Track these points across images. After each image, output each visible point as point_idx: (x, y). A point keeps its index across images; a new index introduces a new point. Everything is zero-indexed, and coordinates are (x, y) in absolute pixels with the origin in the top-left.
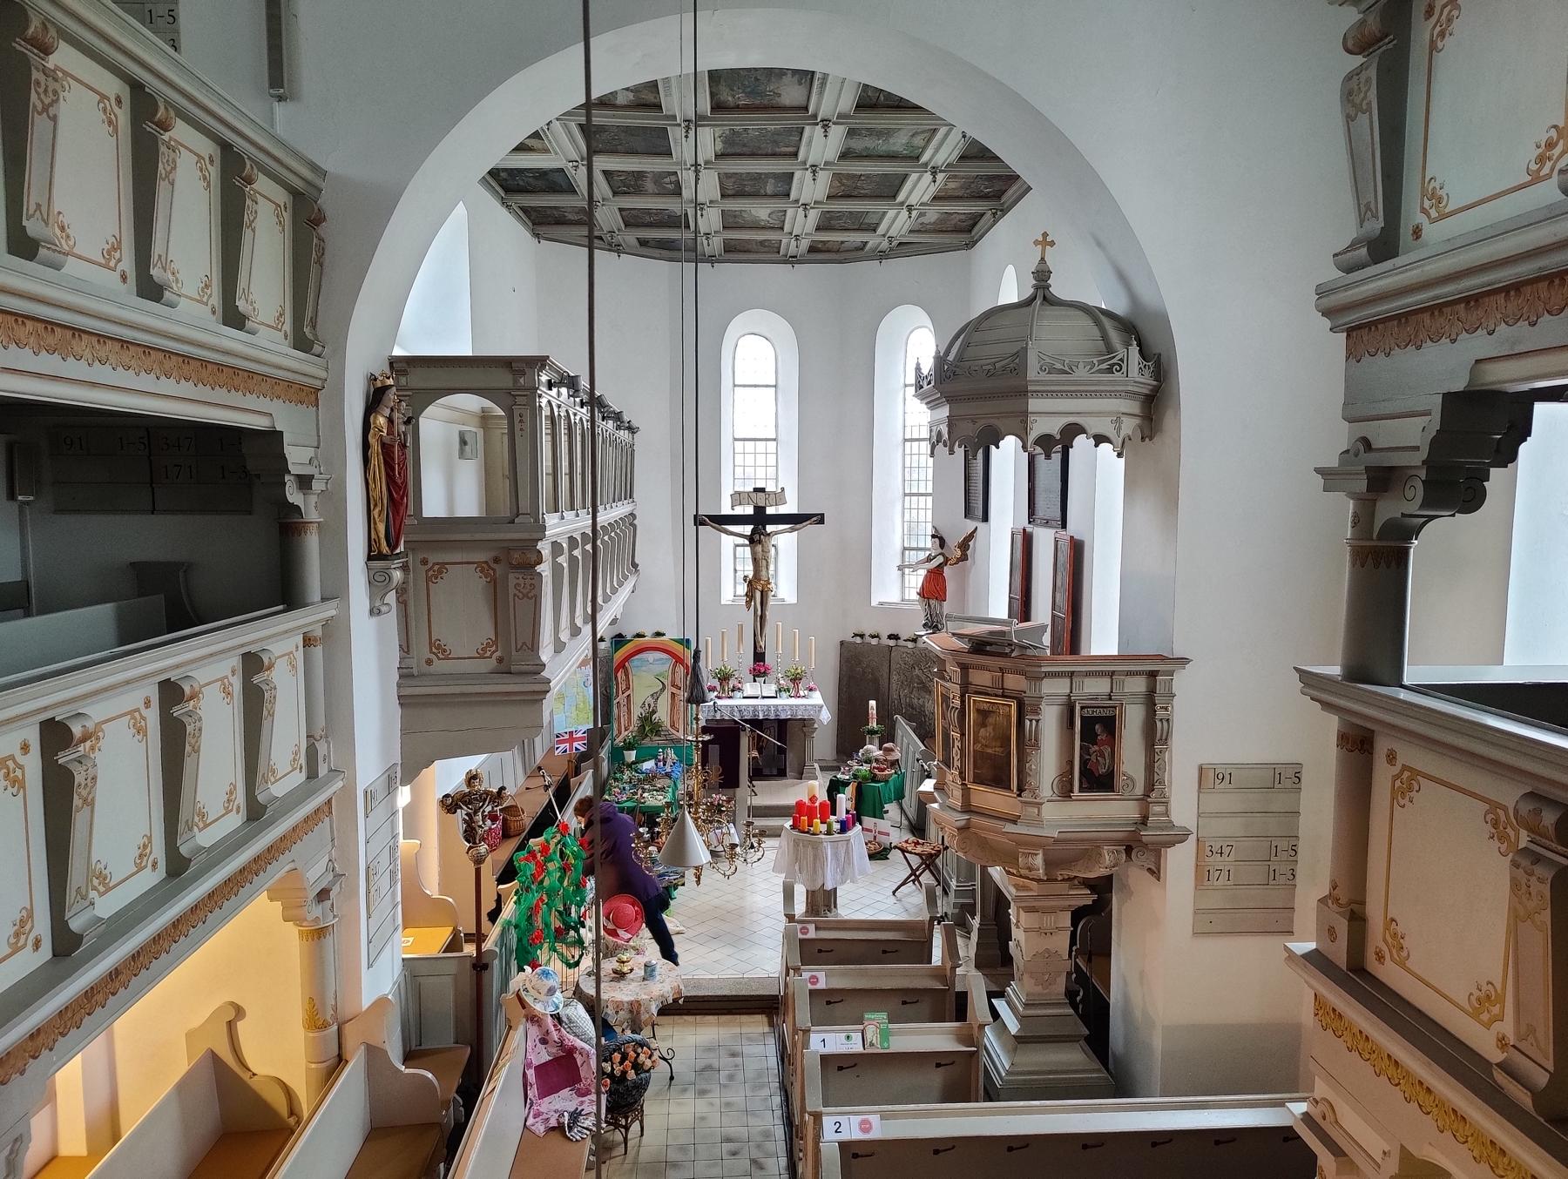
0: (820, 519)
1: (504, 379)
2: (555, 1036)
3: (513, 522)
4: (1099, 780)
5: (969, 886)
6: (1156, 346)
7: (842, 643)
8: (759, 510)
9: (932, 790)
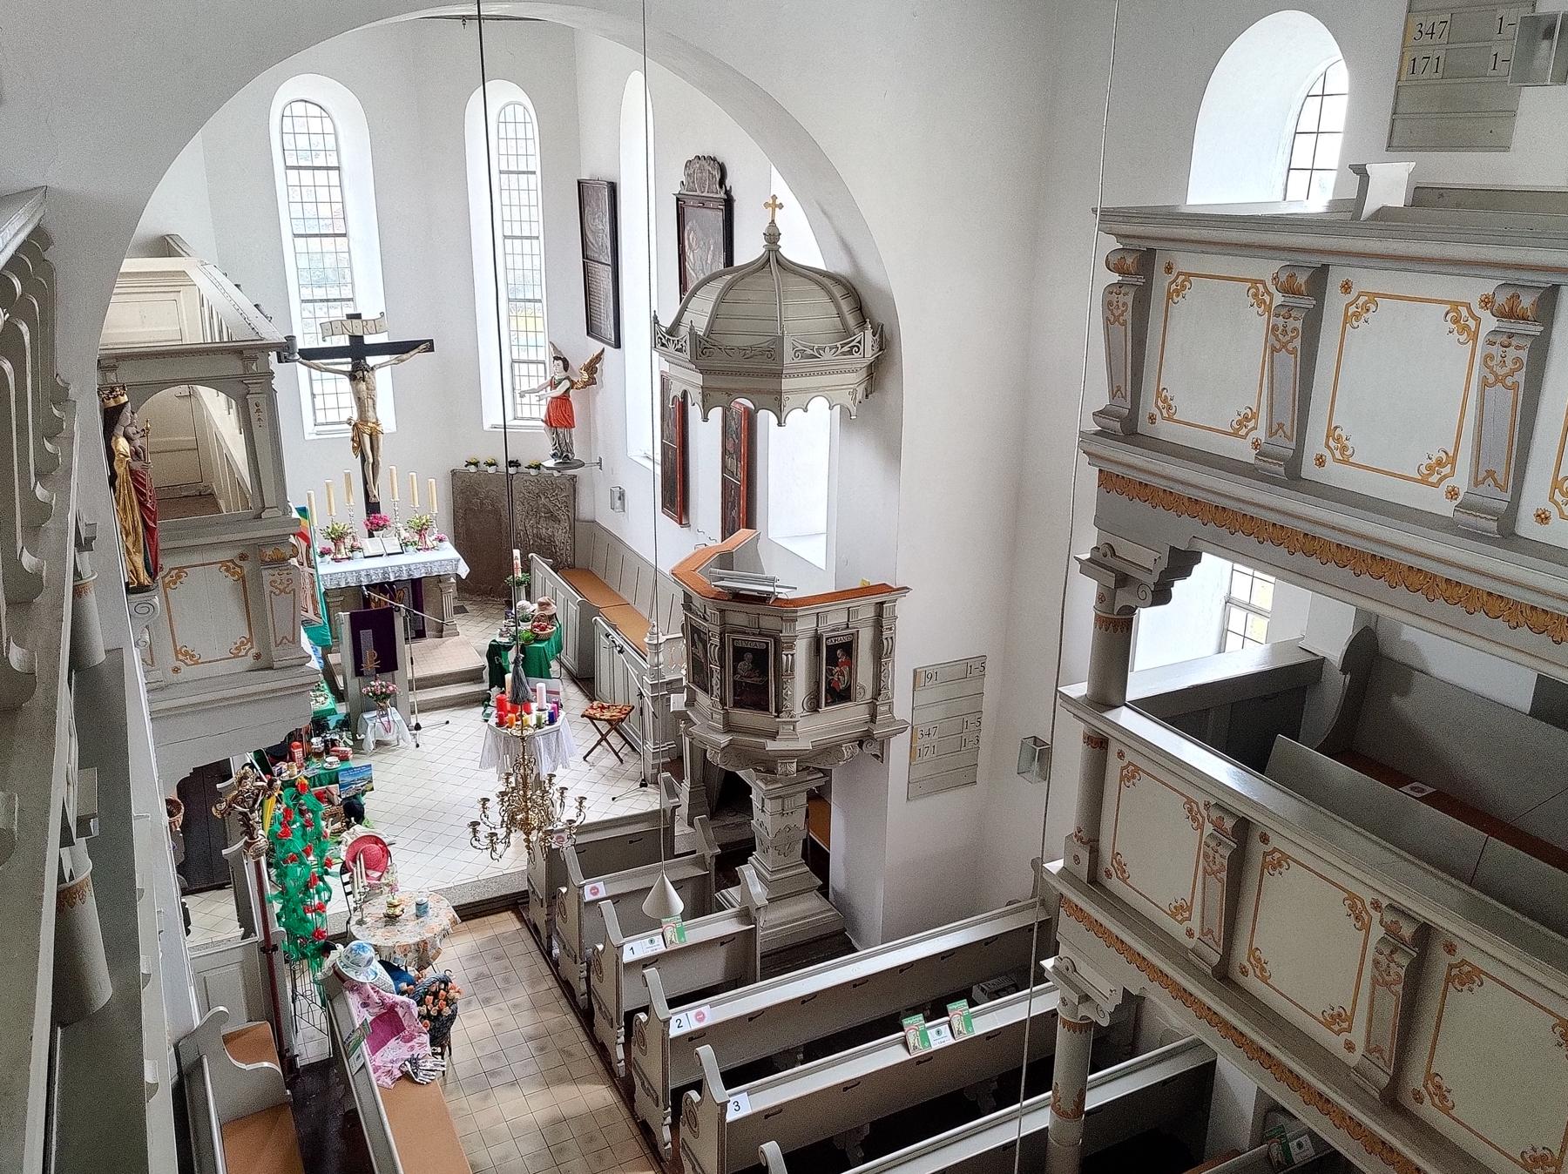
1: (234, 367)
2: (376, 998)
3: (259, 517)
4: (840, 695)
7: (454, 473)
8: (356, 340)
9: (684, 709)
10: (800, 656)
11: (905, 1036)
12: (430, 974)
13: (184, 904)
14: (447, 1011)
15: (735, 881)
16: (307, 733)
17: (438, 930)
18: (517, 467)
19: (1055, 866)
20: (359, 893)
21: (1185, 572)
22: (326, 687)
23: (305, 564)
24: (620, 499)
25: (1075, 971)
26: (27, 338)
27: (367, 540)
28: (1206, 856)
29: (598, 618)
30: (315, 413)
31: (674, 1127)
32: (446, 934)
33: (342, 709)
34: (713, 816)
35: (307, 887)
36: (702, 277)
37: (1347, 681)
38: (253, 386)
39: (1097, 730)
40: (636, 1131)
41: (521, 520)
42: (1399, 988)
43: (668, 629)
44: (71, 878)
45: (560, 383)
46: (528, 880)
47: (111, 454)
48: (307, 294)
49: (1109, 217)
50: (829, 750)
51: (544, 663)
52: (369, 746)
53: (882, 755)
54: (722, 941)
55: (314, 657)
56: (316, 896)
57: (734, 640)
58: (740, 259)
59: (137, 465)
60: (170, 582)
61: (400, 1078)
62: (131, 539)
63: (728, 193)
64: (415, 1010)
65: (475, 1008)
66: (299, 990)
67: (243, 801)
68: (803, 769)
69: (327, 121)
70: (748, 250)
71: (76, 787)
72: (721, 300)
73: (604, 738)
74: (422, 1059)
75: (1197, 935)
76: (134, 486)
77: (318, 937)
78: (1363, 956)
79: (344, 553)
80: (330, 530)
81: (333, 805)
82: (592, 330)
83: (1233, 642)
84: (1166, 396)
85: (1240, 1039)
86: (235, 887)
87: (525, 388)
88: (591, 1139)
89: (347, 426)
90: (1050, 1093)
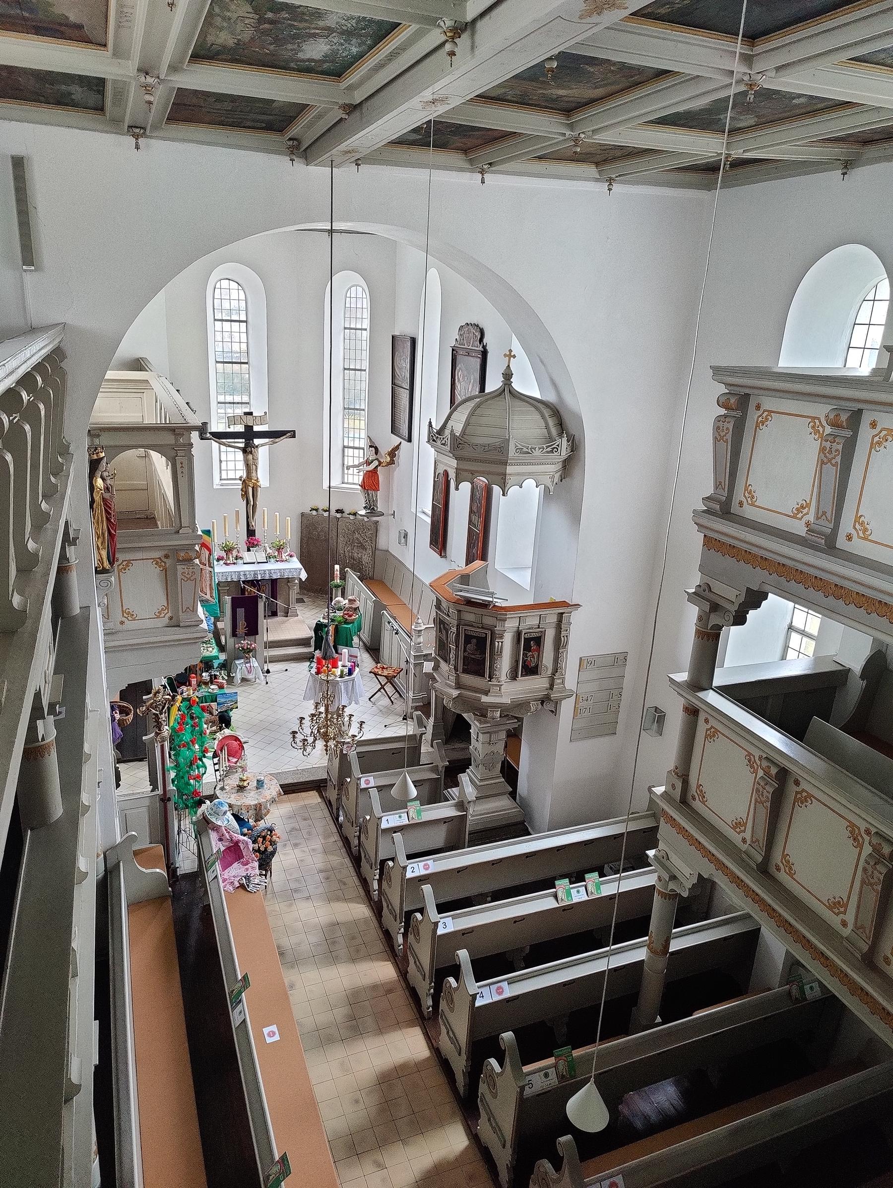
0: (293, 434)
1: (169, 439)
4: (531, 670)
5: (420, 696)
6: (573, 431)
7: (303, 514)
8: (249, 428)
10: (507, 644)
11: (556, 892)
12: (262, 824)
13: (117, 769)
14: (270, 849)
15: (456, 784)
16: (200, 669)
17: (269, 797)
18: (342, 513)
19: (660, 790)
20: (223, 770)
21: (757, 605)
22: (214, 642)
23: (207, 565)
24: (404, 538)
25: (668, 859)
26: (43, 413)
27: (246, 553)
28: (758, 790)
29: (384, 611)
30: (221, 472)
31: (405, 935)
32: (273, 801)
33: (223, 657)
34: (447, 742)
35: (192, 763)
36: (464, 397)
37: (864, 685)
38: (180, 451)
39: (690, 702)
40: (381, 936)
41: (342, 547)
42: (879, 888)
43: (425, 621)
44: (43, 739)
45: (372, 462)
46: (328, 772)
47: (92, 488)
48: (221, 398)
49: (718, 372)
50: (522, 705)
51: (349, 636)
52: (238, 681)
53: (556, 711)
54: (445, 821)
55: (205, 621)
56: (197, 770)
57: (465, 630)
58: (489, 389)
59: (107, 496)
60: (122, 568)
61: (238, 887)
62: (100, 540)
63: (484, 347)
64: (251, 846)
65: (289, 849)
66: (182, 827)
67: (156, 707)
68: (505, 716)
69: (241, 292)
70: (493, 383)
71: (50, 685)
72: (472, 414)
73: (383, 687)
74: (253, 876)
75: (749, 842)
76: (104, 508)
77: (195, 795)
78: (857, 866)
79: (231, 560)
80: (224, 545)
81: (213, 715)
82: (394, 430)
83: (791, 655)
84: (751, 490)
85: (772, 913)
86: (149, 762)
87: (351, 464)
88: (353, 938)
89: (239, 482)
90: (647, 938)
